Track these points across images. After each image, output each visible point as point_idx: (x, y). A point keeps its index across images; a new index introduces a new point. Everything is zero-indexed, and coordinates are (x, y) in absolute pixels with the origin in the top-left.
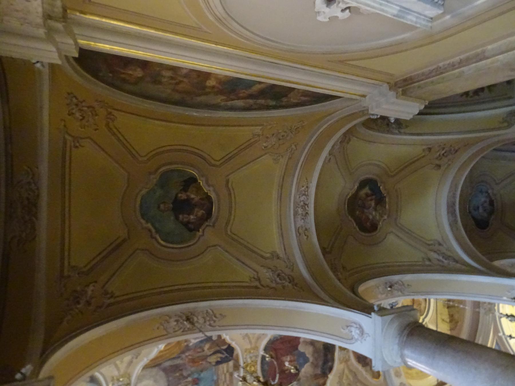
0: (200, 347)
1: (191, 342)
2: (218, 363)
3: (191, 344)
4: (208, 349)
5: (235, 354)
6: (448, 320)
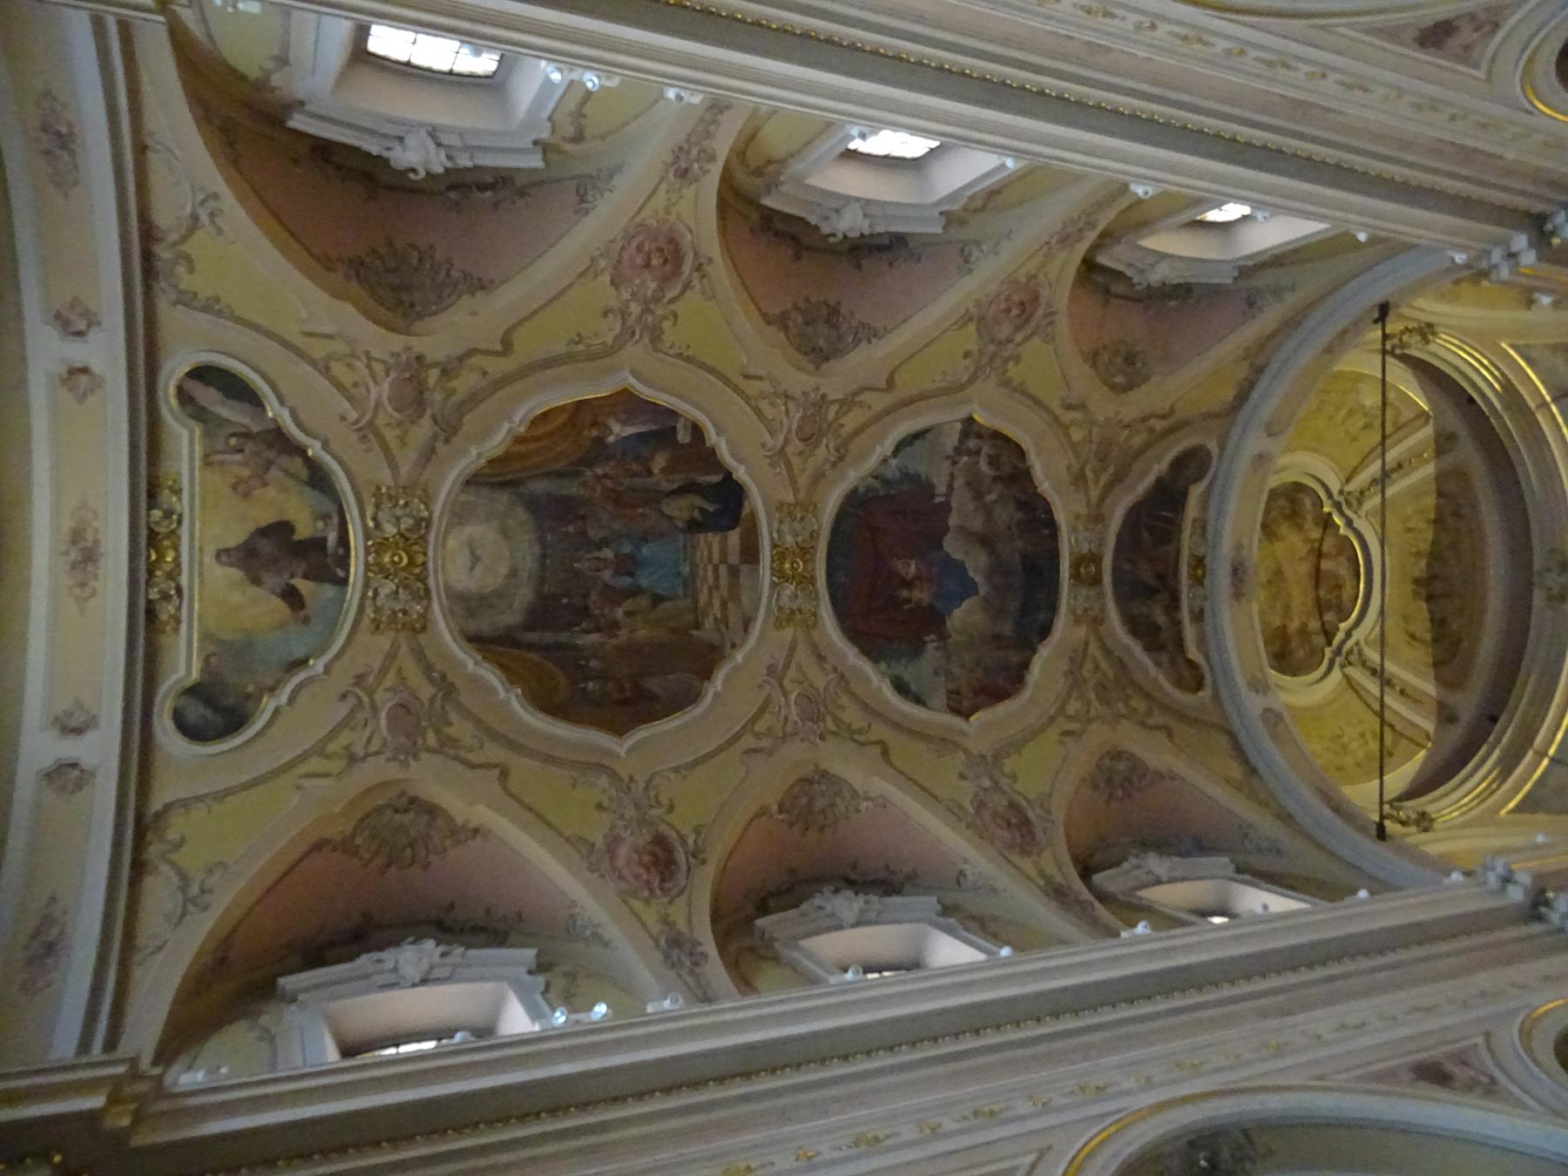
0: (637, 458)
1: (611, 432)
2: (694, 526)
3: (611, 439)
4: (664, 470)
5: (745, 511)
6: (1428, 637)
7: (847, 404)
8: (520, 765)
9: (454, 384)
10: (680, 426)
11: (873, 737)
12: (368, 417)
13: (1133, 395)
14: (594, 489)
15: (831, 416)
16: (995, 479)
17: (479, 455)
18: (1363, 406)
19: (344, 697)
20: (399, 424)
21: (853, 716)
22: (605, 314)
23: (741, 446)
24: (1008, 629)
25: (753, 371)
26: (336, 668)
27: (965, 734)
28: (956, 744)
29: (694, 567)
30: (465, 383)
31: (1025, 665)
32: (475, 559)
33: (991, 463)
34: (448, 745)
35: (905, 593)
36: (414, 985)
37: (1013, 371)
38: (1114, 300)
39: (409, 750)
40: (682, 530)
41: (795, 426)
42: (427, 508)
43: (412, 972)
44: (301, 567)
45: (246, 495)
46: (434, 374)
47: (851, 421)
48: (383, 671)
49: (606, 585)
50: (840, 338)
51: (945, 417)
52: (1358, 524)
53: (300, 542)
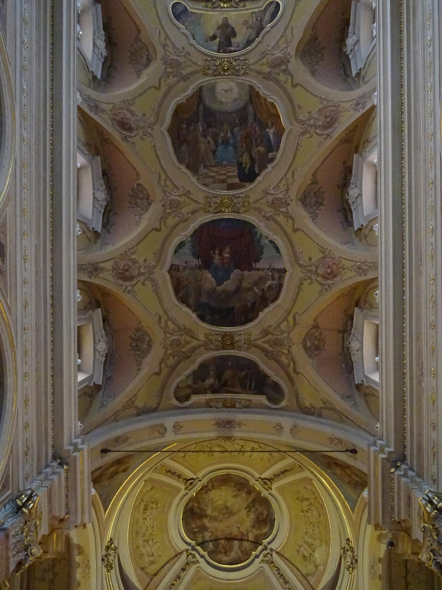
0: (262, 141)
1: (270, 129)
2: (240, 164)
3: (268, 130)
4: (258, 151)
5: (245, 183)
7: (288, 216)
8: (160, 95)
9: (281, 74)
10: (274, 153)
11: (163, 227)
12: (269, 52)
13: (302, 351)
14: (250, 128)
15: (282, 210)
16: (263, 290)
17: (259, 88)
18: (314, 551)
19: (183, 48)
20: (268, 62)
21: (171, 221)
22: (309, 113)
23: (269, 179)
24: (204, 299)
25: (296, 174)
26: (192, 47)
27: (162, 269)
28: (158, 263)
29: (226, 166)
30: (282, 77)
31: (189, 306)
32: (226, 91)
33: (269, 287)
34: (166, 75)
35: (217, 252)
36: (94, 194)
37: (306, 283)
38: (341, 335)
39: (165, 61)
40: (238, 161)
41: (277, 196)
42: (243, 74)
43: (99, 347)
44: (223, 40)
45: (244, 24)
46: (284, 67)
47: (281, 219)
48: (191, 61)
49: (219, 134)
50: (311, 207)
51: (285, 262)
52: (257, 560)
53: (230, 39)
